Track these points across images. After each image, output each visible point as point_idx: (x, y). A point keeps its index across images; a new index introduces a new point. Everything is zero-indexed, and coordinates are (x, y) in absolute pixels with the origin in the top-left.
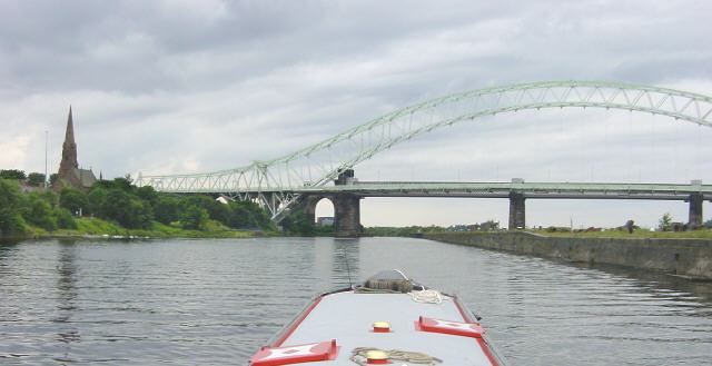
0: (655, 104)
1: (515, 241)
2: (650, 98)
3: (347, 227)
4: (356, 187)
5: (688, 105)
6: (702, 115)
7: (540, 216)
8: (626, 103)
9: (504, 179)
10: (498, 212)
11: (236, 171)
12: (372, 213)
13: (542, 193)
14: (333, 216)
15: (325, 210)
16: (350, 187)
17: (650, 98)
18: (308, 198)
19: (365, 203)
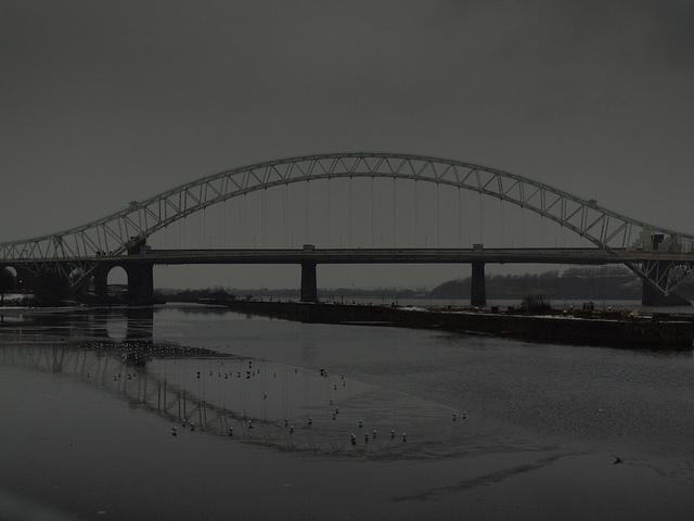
0: (439, 175)
1: (310, 308)
2: (434, 169)
3: (142, 299)
4: (146, 256)
5: (422, 170)
6: (439, 175)
7: (330, 278)
8: (390, 172)
9: (466, 244)
10: (287, 279)
11: (31, 241)
12: (165, 278)
13: (503, 257)
14: (126, 283)
15: (118, 277)
16: (144, 255)
17: (434, 169)
18: (103, 265)
19: (157, 270)
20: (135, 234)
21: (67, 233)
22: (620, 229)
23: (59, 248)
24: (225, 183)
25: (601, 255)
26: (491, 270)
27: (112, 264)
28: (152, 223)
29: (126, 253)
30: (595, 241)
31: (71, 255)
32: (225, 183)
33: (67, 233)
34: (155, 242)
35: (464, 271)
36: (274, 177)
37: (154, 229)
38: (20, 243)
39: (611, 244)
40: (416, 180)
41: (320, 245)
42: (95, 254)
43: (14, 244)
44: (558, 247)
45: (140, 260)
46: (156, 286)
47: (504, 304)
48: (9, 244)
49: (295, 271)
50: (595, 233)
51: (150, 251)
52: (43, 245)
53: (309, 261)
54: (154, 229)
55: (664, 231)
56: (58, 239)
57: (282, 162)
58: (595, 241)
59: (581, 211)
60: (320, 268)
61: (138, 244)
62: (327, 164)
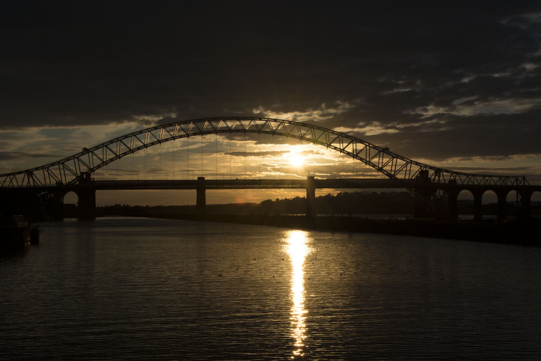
20: (84, 169)
21: (37, 169)
23: (31, 179)
28: (98, 162)
30: (388, 174)
31: (39, 184)
33: (37, 169)
34: (95, 177)
37: (99, 167)
52: (20, 177)
54: (99, 167)
56: (29, 173)
58: (388, 174)
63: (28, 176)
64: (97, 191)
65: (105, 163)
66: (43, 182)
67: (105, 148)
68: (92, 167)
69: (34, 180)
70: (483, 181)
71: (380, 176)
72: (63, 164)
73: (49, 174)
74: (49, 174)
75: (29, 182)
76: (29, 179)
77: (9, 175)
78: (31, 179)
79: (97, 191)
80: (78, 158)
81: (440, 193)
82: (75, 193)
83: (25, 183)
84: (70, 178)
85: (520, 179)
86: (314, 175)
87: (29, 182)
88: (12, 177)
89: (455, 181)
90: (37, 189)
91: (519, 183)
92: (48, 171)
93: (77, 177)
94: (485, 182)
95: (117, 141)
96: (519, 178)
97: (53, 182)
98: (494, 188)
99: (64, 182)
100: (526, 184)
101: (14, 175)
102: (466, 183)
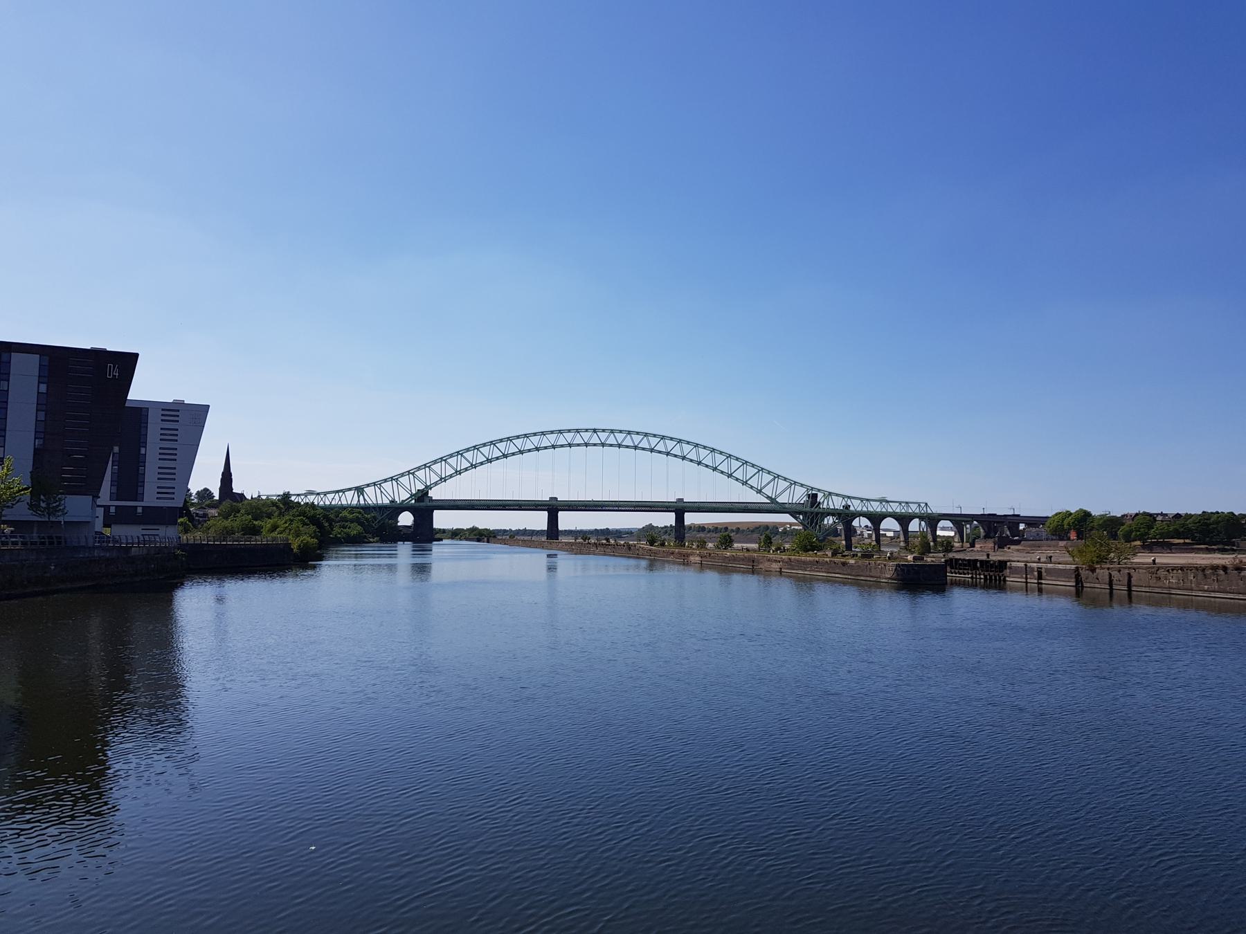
4: (429, 504)
7: (567, 521)
10: (539, 521)
15: (406, 519)
16: (426, 503)
18: (395, 509)
19: (437, 514)
20: (421, 487)
21: (368, 485)
22: (765, 487)
23: (361, 497)
24: (490, 455)
25: (774, 507)
26: (690, 519)
27: (828, 514)
28: (435, 478)
29: (413, 501)
30: (768, 497)
31: (370, 502)
32: (490, 455)
33: (368, 485)
34: (435, 494)
35: (668, 519)
36: (513, 449)
37: (436, 484)
38: (329, 493)
39: (780, 500)
40: (651, 452)
41: (561, 498)
42: (388, 502)
43: (325, 494)
44: (611, 500)
45: (423, 506)
46: (434, 527)
47: (409, 543)
48: (302, 495)
49: (544, 515)
50: (768, 491)
51: (431, 499)
52: (349, 494)
53: (553, 508)
54: (436, 484)
55: (819, 490)
56: (360, 490)
57: (518, 437)
58: (768, 497)
59: (732, 471)
60: (560, 514)
61: (422, 495)
62: (552, 438)
63: (358, 494)
64: (686, 513)
65: (443, 480)
66: (375, 502)
67: (443, 462)
68: (428, 484)
69: (365, 500)
70: (879, 507)
71: (760, 499)
72: (413, 474)
73: (381, 492)
74: (381, 492)
75: (359, 501)
76: (359, 497)
77: (338, 492)
78: (361, 497)
79: (686, 513)
80: (413, 474)
81: (829, 521)
82: (602, 528)
83: (355, 502)
84: (404, 496)
85: (923, 505)
86: (316, 513)
87: (359, 501)
88: (341, 494)
89: (847, 507)
90: (367, 508)
91: (921, 509)
92: (380, 489)
93: (412, 495)
94: (928, 509)
95: (457, 455)
96: (921, 504)
97: (386, 501)
98: (895, 516)
99: (397, 499)
100: (929, 511)
101: (344, 492)
102: (859, 509)
